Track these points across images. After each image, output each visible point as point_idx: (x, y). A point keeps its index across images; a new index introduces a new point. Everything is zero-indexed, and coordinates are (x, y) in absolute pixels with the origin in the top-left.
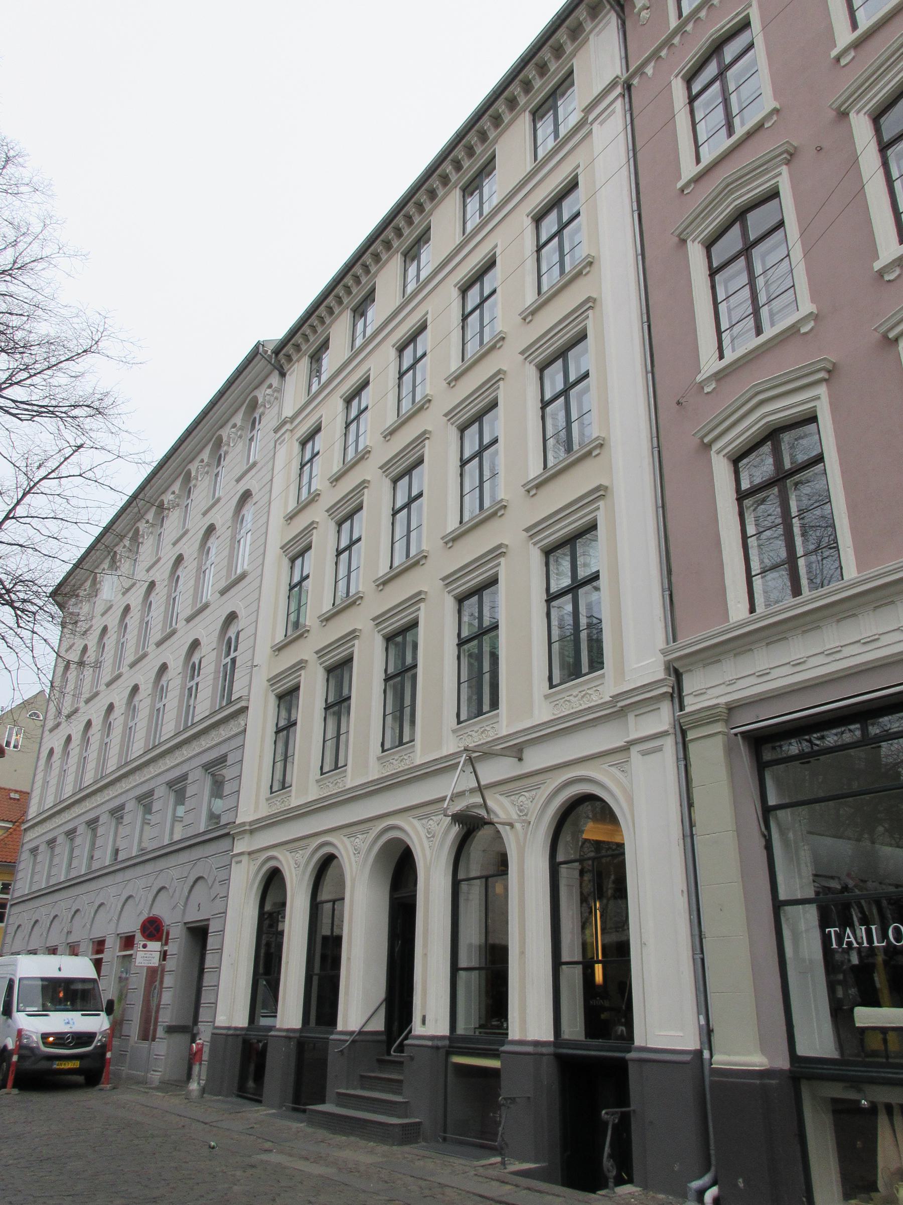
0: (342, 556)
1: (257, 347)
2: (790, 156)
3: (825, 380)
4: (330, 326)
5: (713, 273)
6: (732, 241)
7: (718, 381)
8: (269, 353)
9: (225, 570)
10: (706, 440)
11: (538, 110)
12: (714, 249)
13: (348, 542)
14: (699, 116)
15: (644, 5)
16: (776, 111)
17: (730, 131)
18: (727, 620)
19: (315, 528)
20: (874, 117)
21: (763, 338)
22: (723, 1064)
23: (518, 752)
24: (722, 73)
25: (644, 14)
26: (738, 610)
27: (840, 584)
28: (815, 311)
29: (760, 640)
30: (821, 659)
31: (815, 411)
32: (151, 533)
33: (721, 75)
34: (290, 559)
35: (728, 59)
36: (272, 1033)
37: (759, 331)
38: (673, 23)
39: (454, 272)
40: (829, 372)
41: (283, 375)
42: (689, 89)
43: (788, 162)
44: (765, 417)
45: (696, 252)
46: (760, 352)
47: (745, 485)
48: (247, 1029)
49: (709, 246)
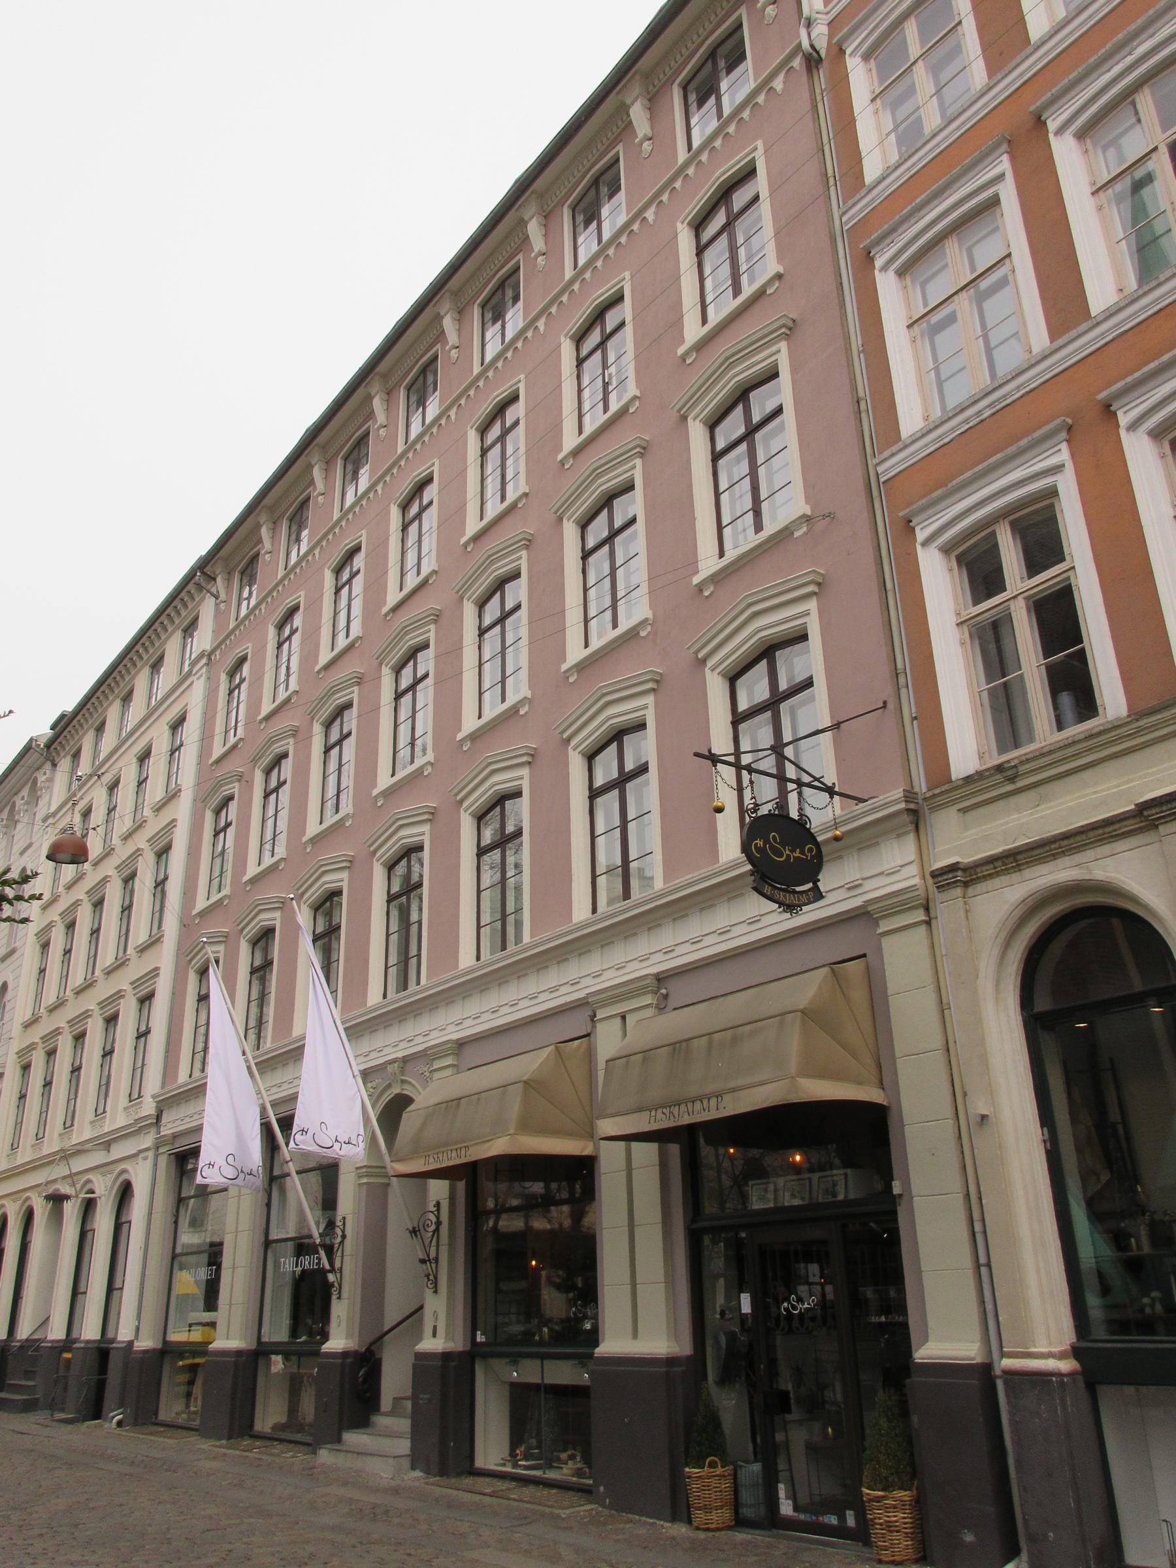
0: (403, 700)
1: (31, 740)
2: (790, 330)
3: (654, 690)
4: (164, 643)
5: (716, 457)
6: (733, 426)
7: (201, 917)
8: (42, 746)
9: (6, 938)
10: (700, 656)
11: (349, 455)
12: (718, 430)
13: (411, 681)
14: (707, 270)
15: (645, 135)
16: (779, 276)
17: (737, 291)
18: (457, 966)
19: (141, 855)
20: (710, 424)
21: (764, 535)
22: (951, 1359)
23: (107, 1145)
24: (730, 224)
25: (647, 146)
26: (581, 911)
27: (174, 1086)
28: (809, 513)
29: (722, 895)
30: (744, 928)
31: (806, 628)
32: (27, 811)
33: (728, 226)
34: (123, 880)
35: (736, 207)
36: (114, 1345)
37: (758, 527)
38: (477, 369)
39: (126, 754)
40: (819, 584)
41: (54, 765)
42: (697, 237)
43: (787, 337)
44: (756, 633)
45: (697, 432)
46: (728, 572)
47: (743, 706)
48: (100, 1341)
49: (712, 426)
